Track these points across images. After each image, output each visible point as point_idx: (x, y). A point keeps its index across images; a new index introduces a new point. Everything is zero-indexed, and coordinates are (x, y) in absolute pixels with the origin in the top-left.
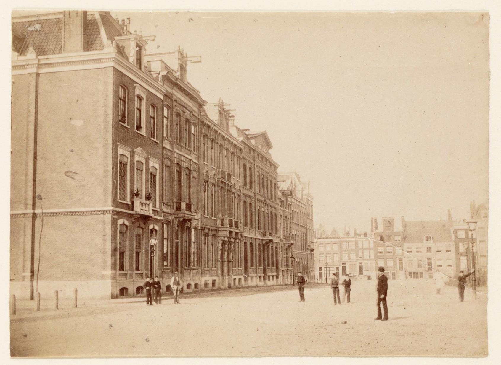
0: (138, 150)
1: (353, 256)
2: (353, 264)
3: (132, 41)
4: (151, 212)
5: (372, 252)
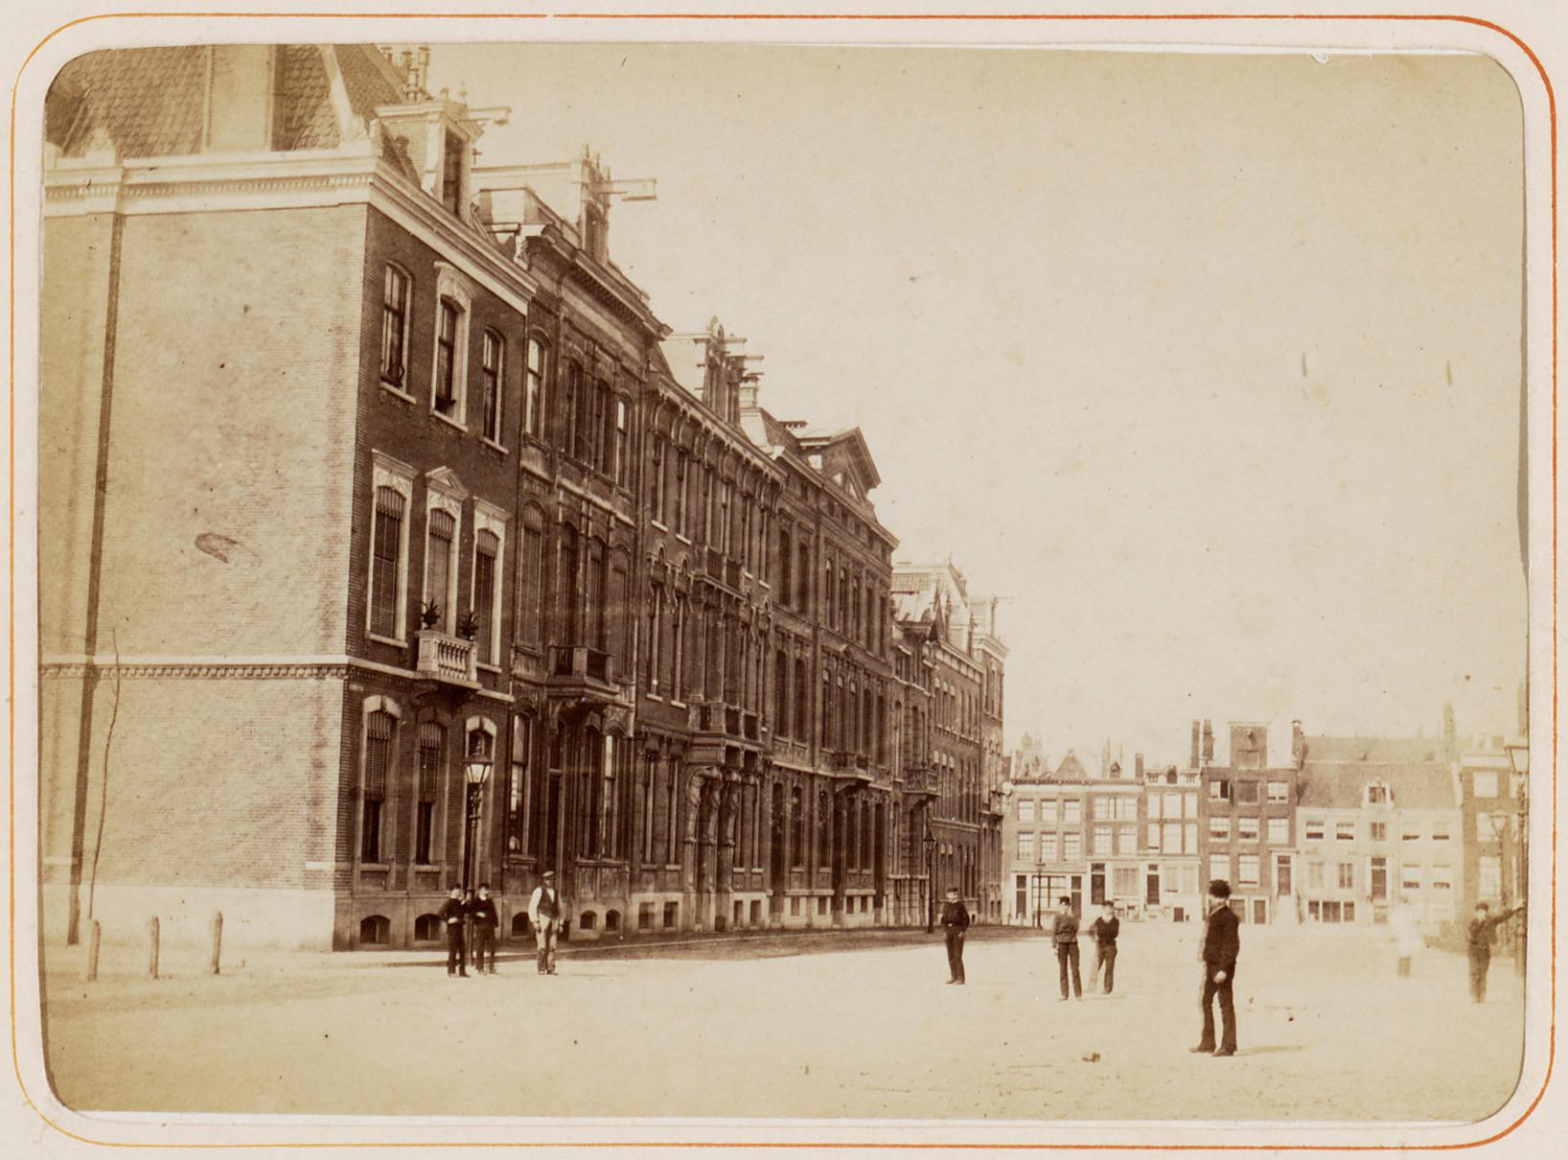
0: (439, 473)
1: (1129, 843)
2: (1126, 870)
3: (432, 122)
4: (474, 675)
5: (1192, 831)
